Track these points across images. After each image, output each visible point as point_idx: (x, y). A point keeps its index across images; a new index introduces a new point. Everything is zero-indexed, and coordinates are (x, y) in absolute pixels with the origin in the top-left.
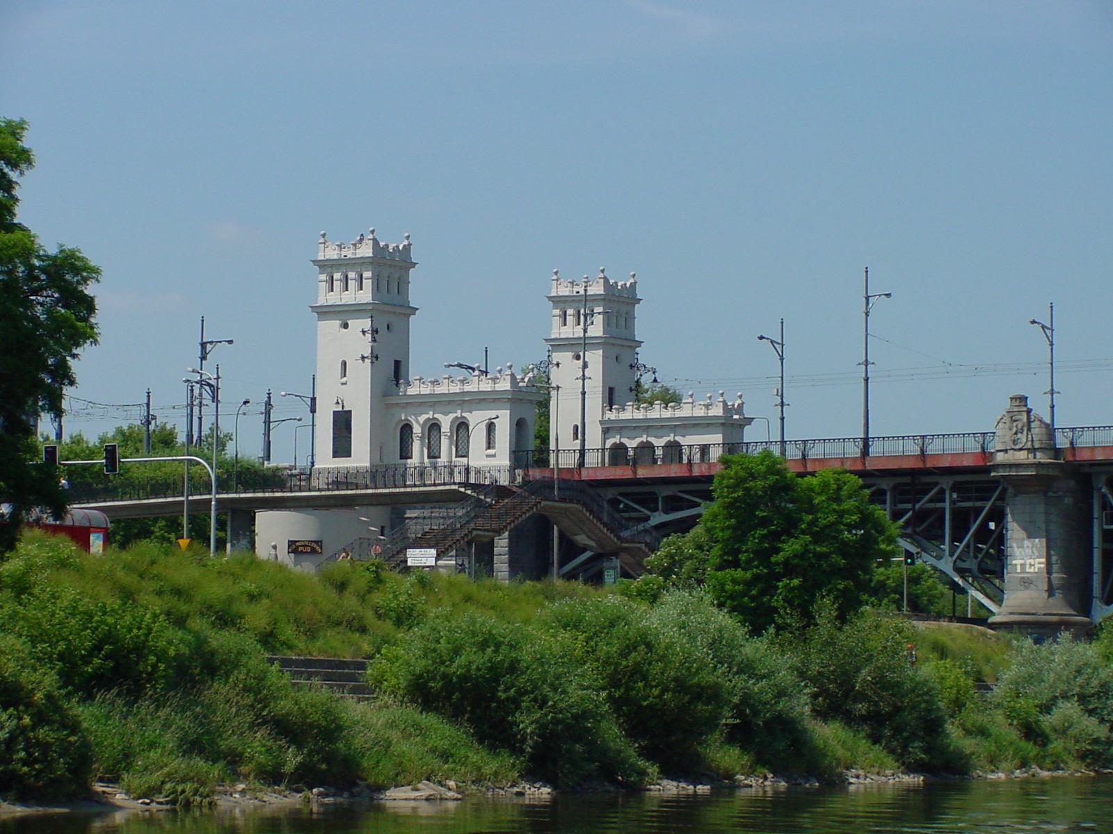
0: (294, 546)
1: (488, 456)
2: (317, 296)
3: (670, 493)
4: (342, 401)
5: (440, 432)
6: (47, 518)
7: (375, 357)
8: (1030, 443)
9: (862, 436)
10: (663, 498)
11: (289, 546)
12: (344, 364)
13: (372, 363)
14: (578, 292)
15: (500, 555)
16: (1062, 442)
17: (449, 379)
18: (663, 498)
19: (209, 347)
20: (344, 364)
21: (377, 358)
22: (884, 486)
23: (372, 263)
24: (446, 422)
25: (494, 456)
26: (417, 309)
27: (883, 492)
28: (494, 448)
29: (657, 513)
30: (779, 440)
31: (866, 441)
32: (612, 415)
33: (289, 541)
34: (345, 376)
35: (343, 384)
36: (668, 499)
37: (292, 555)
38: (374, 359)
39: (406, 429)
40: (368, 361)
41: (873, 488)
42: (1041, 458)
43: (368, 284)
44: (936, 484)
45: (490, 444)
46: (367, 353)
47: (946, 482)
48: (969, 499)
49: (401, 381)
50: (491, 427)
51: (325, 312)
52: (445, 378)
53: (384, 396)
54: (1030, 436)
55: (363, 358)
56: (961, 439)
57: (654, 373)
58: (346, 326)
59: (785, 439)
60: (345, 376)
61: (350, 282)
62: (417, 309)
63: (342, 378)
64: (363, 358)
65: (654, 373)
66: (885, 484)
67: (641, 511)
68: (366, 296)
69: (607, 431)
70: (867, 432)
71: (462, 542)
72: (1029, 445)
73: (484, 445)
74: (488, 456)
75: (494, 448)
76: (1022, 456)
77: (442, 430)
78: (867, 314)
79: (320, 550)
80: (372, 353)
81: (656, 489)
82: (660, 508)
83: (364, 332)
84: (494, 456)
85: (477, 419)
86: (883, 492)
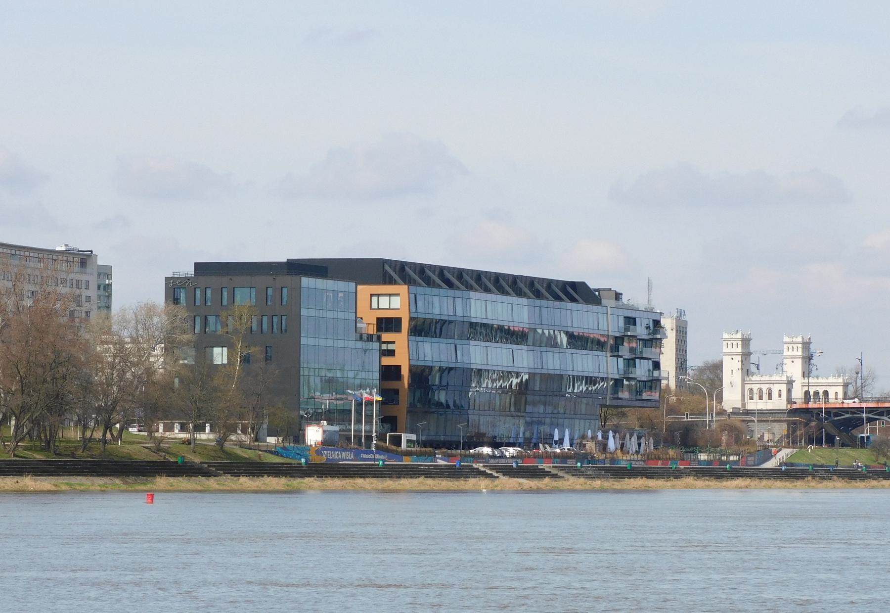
39: (751, 390)
45: (780, 396)
73: (778, 396)
81: (813, 411)
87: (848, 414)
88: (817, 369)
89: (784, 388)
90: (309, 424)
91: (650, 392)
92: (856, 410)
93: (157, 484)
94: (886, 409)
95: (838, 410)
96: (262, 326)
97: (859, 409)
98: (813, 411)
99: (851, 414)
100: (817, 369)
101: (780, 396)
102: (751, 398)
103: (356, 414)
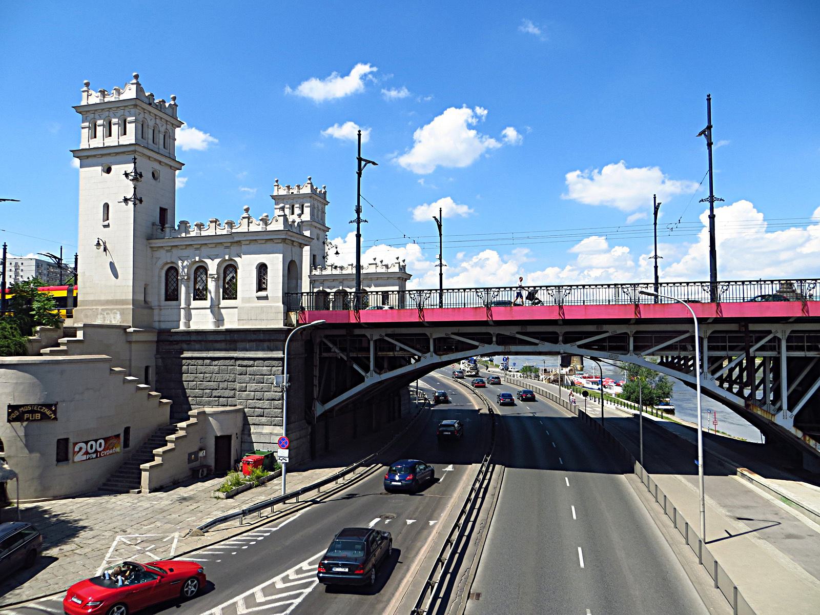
0: (17, 413)
1: (259, 298)
2: (80, 142)
3: (443, 335)
4: (104, 243)
5: (206, 274)
7: (137, 200)
9: (654, 282)
10: (434, 340)
11: (9, 414)
12: (106, 206)
13: (135, 204)
14: (292, 193)
15: (273, 400)
17: (215, 222)
18: (434, 340)
19: (363, 163)
20: (106, 206)
21: (141, 201)
24: (213, 266)
25: (266, 298)
26: (184, 164)
28: (266, 289)
29: (428, 355)
31: (714, 283)
32: (317, 272)
33: (10, 406)
34: (108, 219)
35: (105, 226)
36: (437, 341)
37: (17, 424)
38: (137, 202)
39: (172, 271)
40: (131, 204)
43: (131, 128)
44: (769, 332)
45: (261, 286)
46: (130, 195)
48: (801, 349)
49: (166, 226)
50: (262, 269)
51: (87, 157)
52: (211, 222)
53: (147, 240)
56: (612, 291)
57: (336, 248)
60: (108, 219)
62: (184, 164)
63: (104, 221)
64: (126, 200)
65: (336, 248)
67: (409, 352)
68: (130, 138)
69: (313, 282)
70: (657, 277)
73: (254, 286)
74: (259, 298)
75: (266, 289)
77: (209, 272)
79: (53, 416)
80: (135, 194)
81: (427, 331)
82: (432, 349)
84: (266, 298)
85: (247, 265)
87: (490, 342)
88: (337, 253)
89: (275, 263)
90: (748, 329)
91: (397, 92)
92: (518, 329)
93: (582, 261)
94: (789, 329)
95: (455, 329)
96: (265, 425)
97: (531, 329)
98: (427, 331)
99: (498, 343)
100: (337, 253)
101: (261, 286)
102: (200, 295)
103: (240, 345)
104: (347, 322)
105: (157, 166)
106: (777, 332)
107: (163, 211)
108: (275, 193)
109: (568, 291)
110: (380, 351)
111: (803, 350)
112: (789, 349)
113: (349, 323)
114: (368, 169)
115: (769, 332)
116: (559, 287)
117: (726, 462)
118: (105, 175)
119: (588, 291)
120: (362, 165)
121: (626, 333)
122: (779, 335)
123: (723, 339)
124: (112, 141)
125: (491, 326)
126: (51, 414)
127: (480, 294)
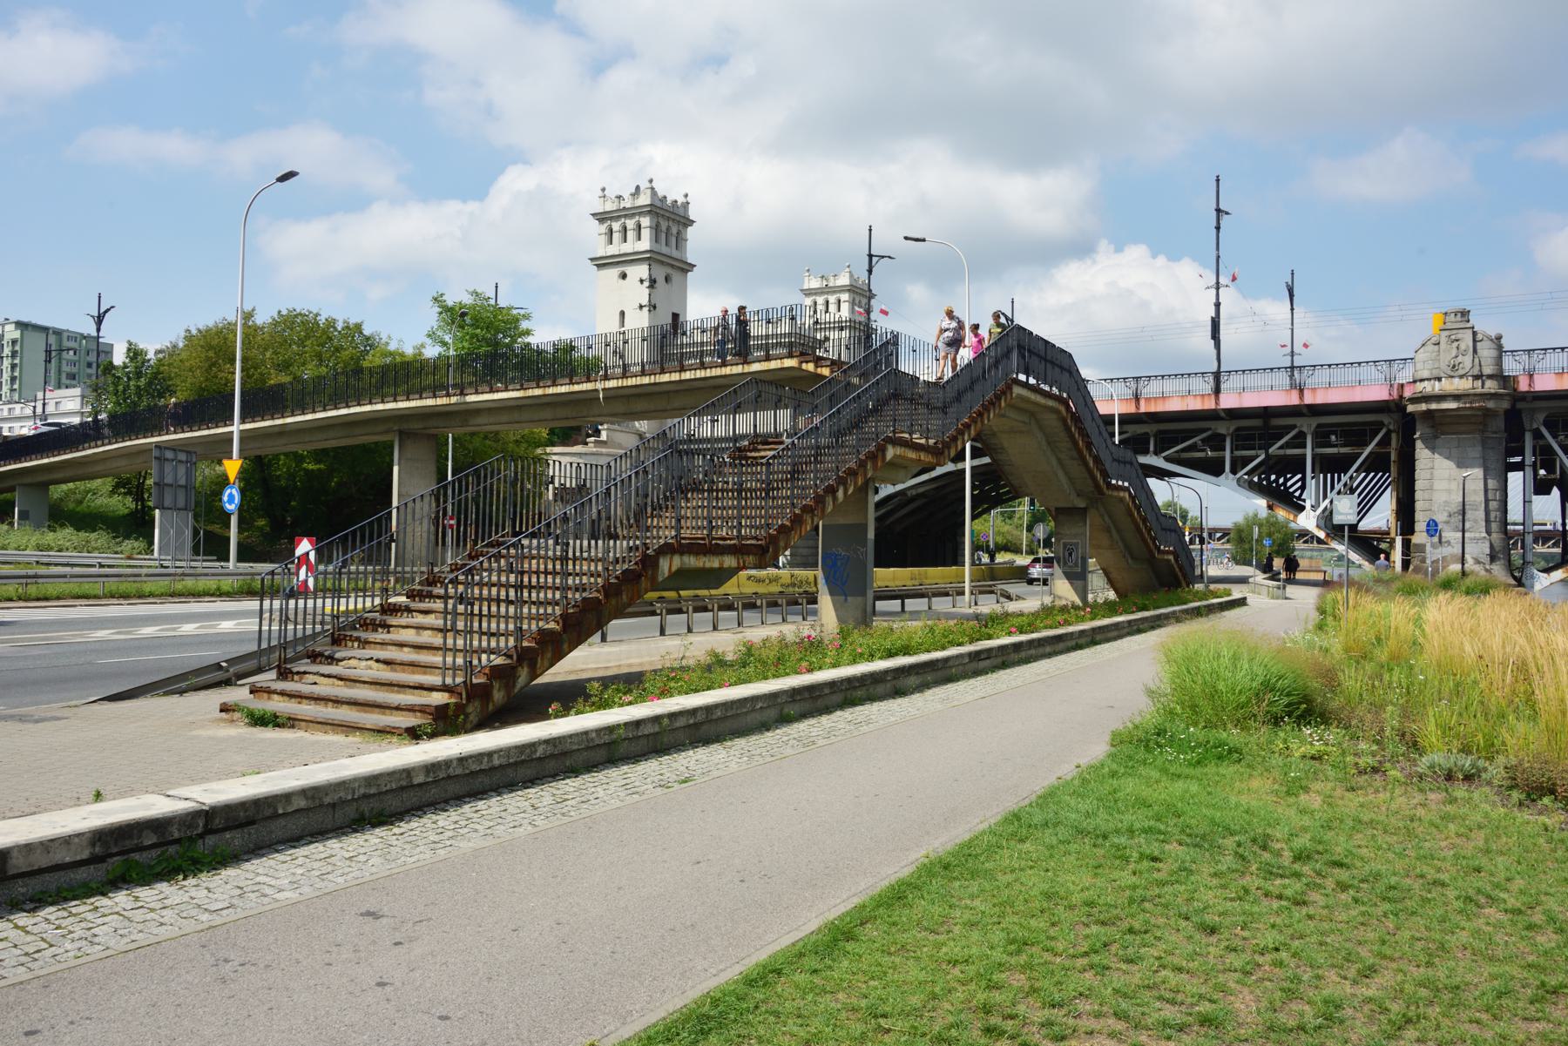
6: (1390, 423)
8: (1477, 368)
12: (622, 314)
13: (650, 311)
16: (1511, 366)
19: (875, 259)
20: (622, 314)
21: (655, 307)
22: (1222, 431)
23: (650, 212)
27: (1222, 438)
30: (1289, 365)
40: (646, 310)
41: (1209, 433)
42: (1491, 387)
43: (646, 233)
44: (1294, 427)
46: (645, 301)
47: (1307, 425)
51: (602, 263)
54: (1477, 361)
55: (641, 307)
58: (624, 276)
59: (1295, 364)
61: (642, 230)
66: (1222, 428)
71: (840, 494)
72: (1476, 371)
76: (1447, 386)
78: (1218, 228)
80: (650, 301)
83: (642, 281)
86: (1222, 438)
94: (1314, 422)
104: (1213, 407)
105: (670, 271)
106: (1302, 426)
107: (675, 316)
108: (806, 287)
109: (1541, 357)
110: (1237, 450)
111: (1254, 449)
112: (1316, 445)
113: (1215, 411)
114: (1225, 220)
115: (1294, 427)
116: (1137, 379)
117: (994, 585)
118: (621, 281)
119: (1334, 371)
120: (874, 262)
121: (1147, 433)
122: (1305, 429)
123: (1252, 438)
124: (628, 248)
125: (1222, 419)
126: (721, 564)
127: (1379, 368)
